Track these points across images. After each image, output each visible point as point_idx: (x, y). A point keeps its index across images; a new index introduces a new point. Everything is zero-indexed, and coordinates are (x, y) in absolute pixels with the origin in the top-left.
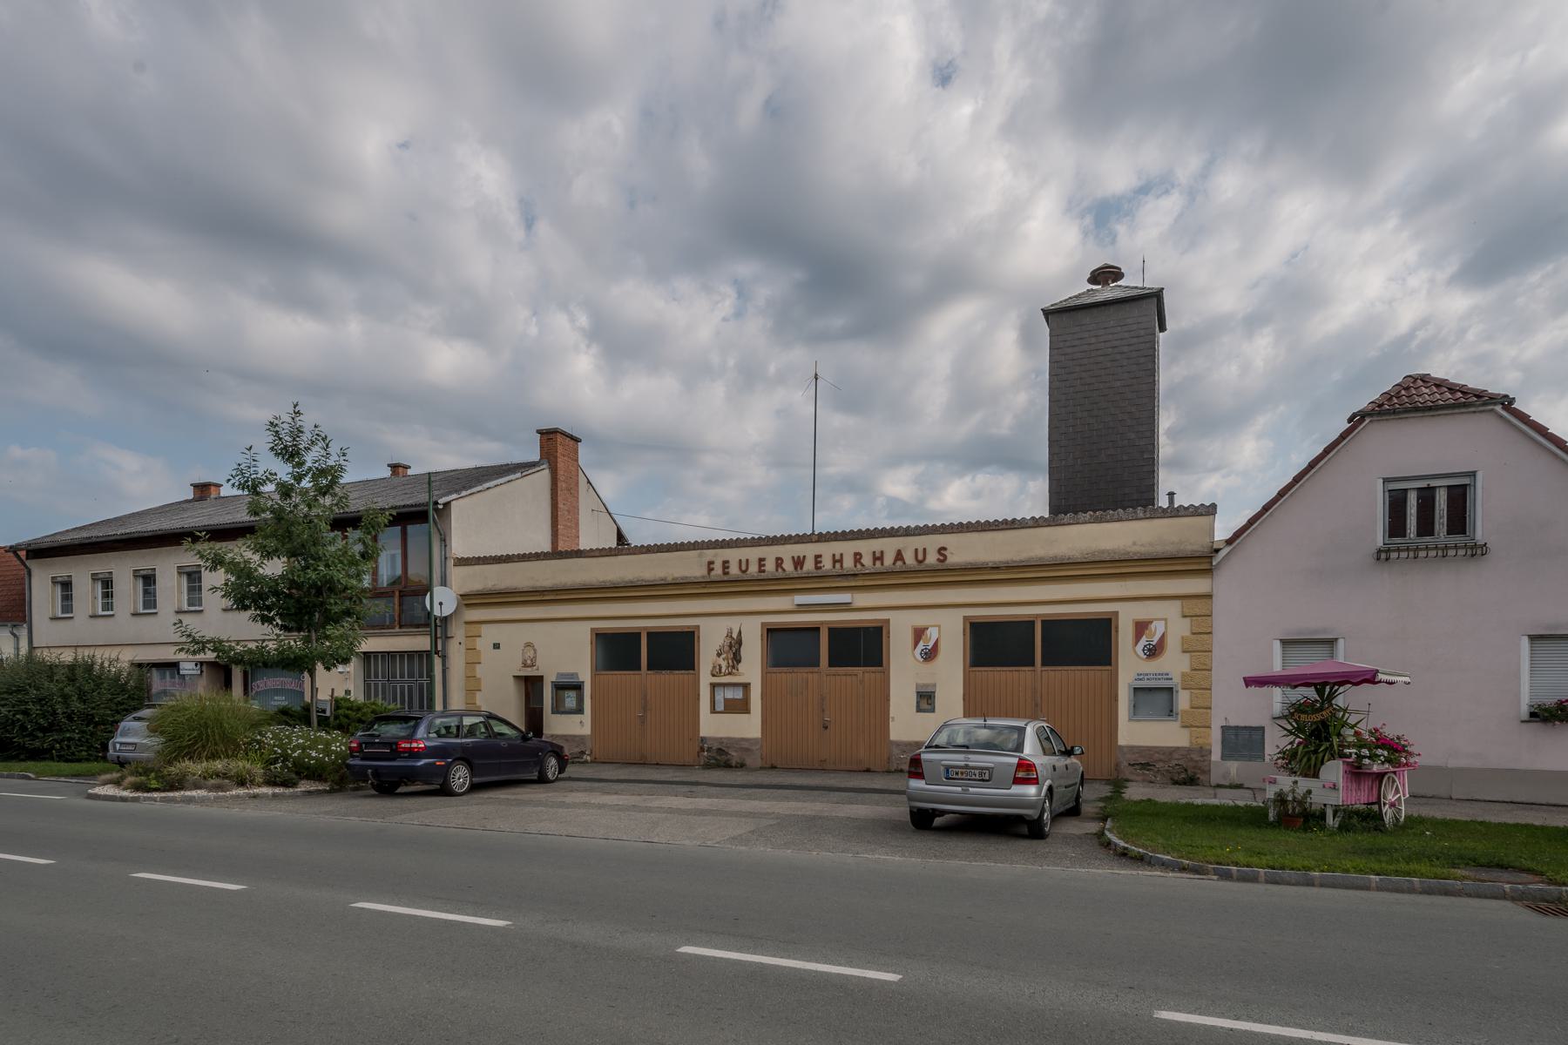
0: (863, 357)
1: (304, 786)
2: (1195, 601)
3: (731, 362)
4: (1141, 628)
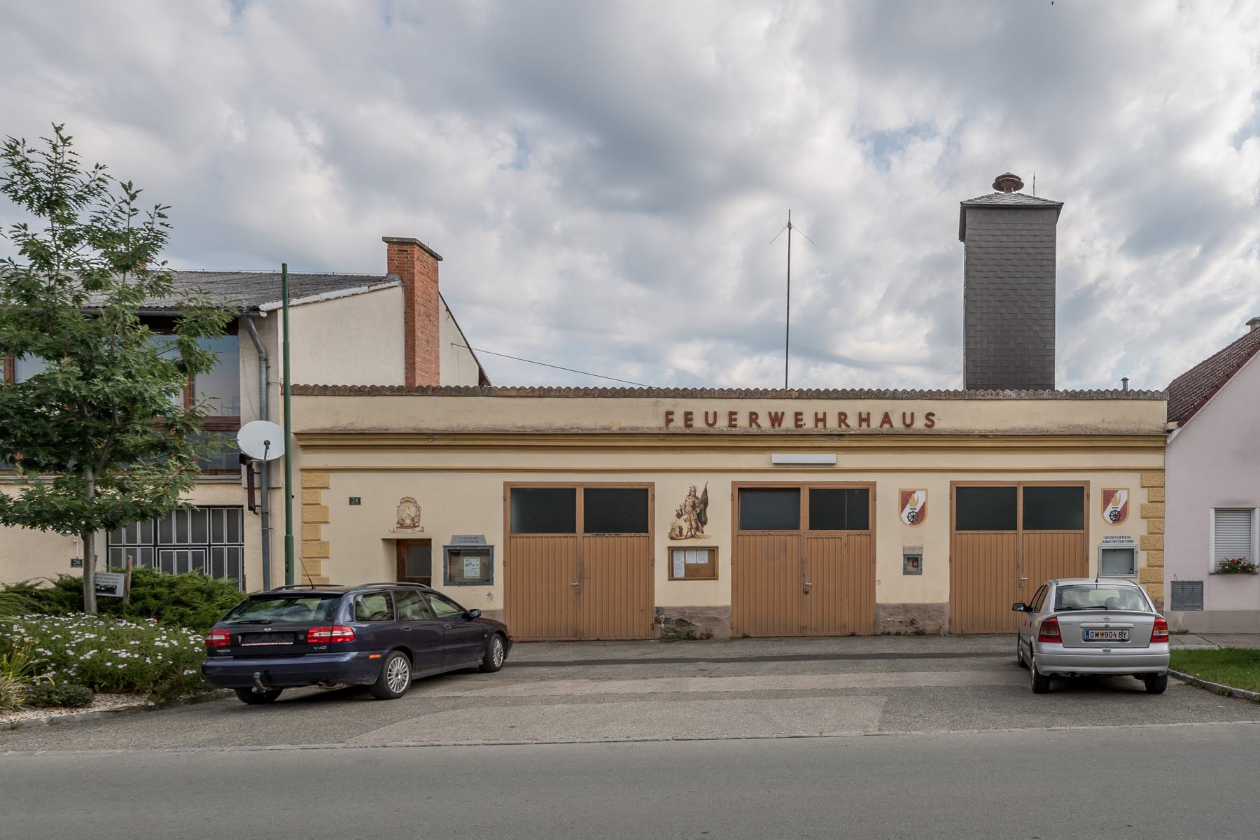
0: (657, 232)
1: (103, 704)
2: (1151, 474)
3: (508, 213)
4: (1108, 496)
